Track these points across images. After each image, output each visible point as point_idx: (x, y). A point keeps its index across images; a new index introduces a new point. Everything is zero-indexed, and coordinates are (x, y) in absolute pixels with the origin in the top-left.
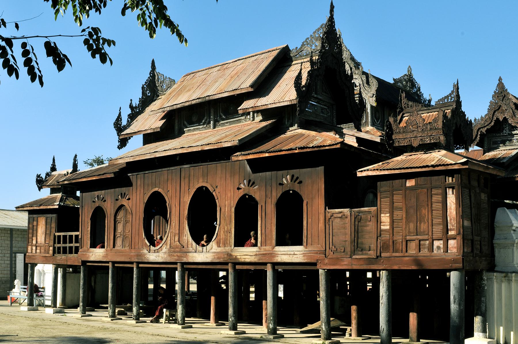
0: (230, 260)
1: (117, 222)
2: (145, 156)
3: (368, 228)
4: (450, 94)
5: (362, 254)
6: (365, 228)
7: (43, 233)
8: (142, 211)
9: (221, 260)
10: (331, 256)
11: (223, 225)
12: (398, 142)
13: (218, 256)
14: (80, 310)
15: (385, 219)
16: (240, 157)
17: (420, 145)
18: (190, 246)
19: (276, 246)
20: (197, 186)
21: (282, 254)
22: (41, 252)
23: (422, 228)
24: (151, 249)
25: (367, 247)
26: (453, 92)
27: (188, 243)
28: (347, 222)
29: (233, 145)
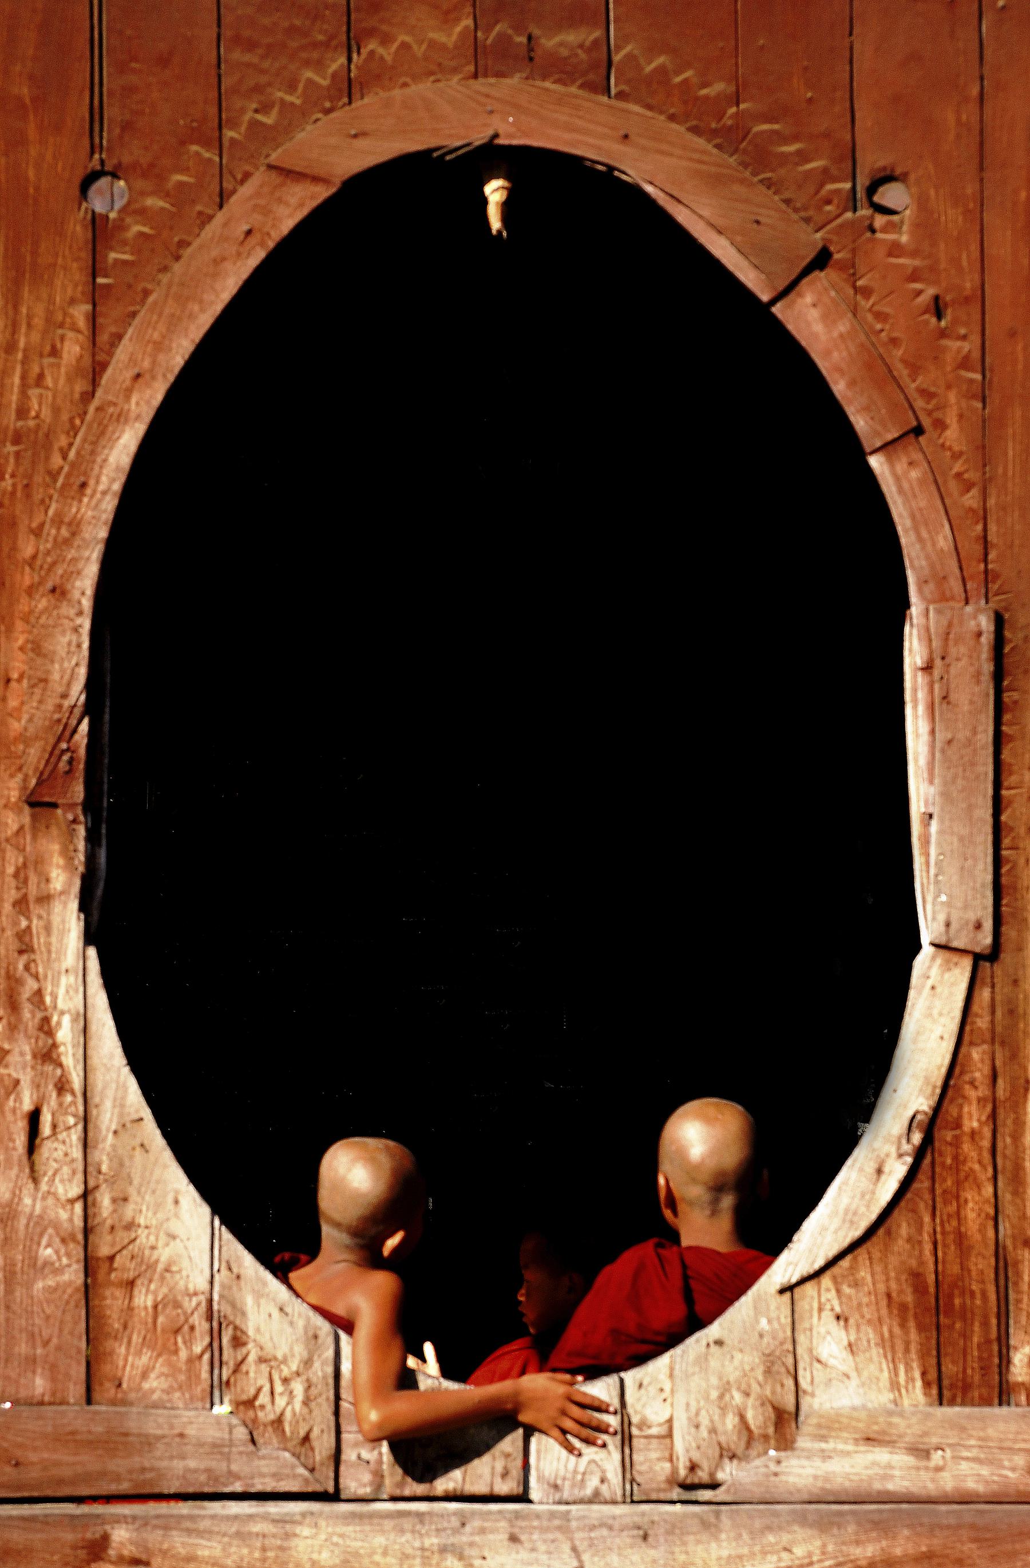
27: (112, 1301)
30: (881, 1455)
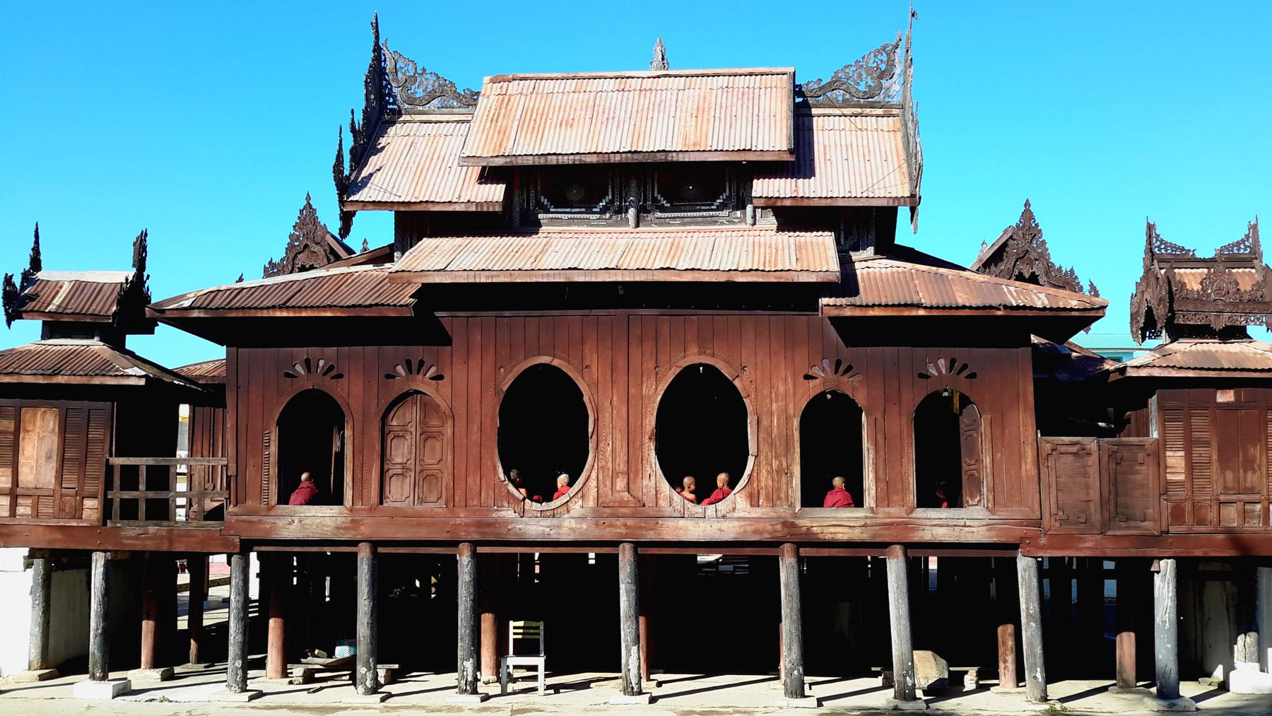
0: (792, 537)
1: (392, 435)
2: (533, 275)
3: (1138, 477)
4: (1243, 241)
5: (1128, 528)
6: (1133, 477)
7: (49, 458)
8: (495, 410)
9: (766, 537)
10: (1055, 530)
11: (767, 455)
12: (1184, 316)
13: (757, 526)
14: (236, 680)
15: (1174, 461)
16: (846, 310)
17: (1227, 327)
18: (662, 503)
19: (918, 507)
20: (685, 363)
21: (935, 525)
22: (36, 514)
23: (1249, 480)
24: (526, 507)
25: (1138, 514)
26: (1247, 236)
27: (659, 495)
28: (1089, 464)
29: (825, 280)
30: (744, 513)
